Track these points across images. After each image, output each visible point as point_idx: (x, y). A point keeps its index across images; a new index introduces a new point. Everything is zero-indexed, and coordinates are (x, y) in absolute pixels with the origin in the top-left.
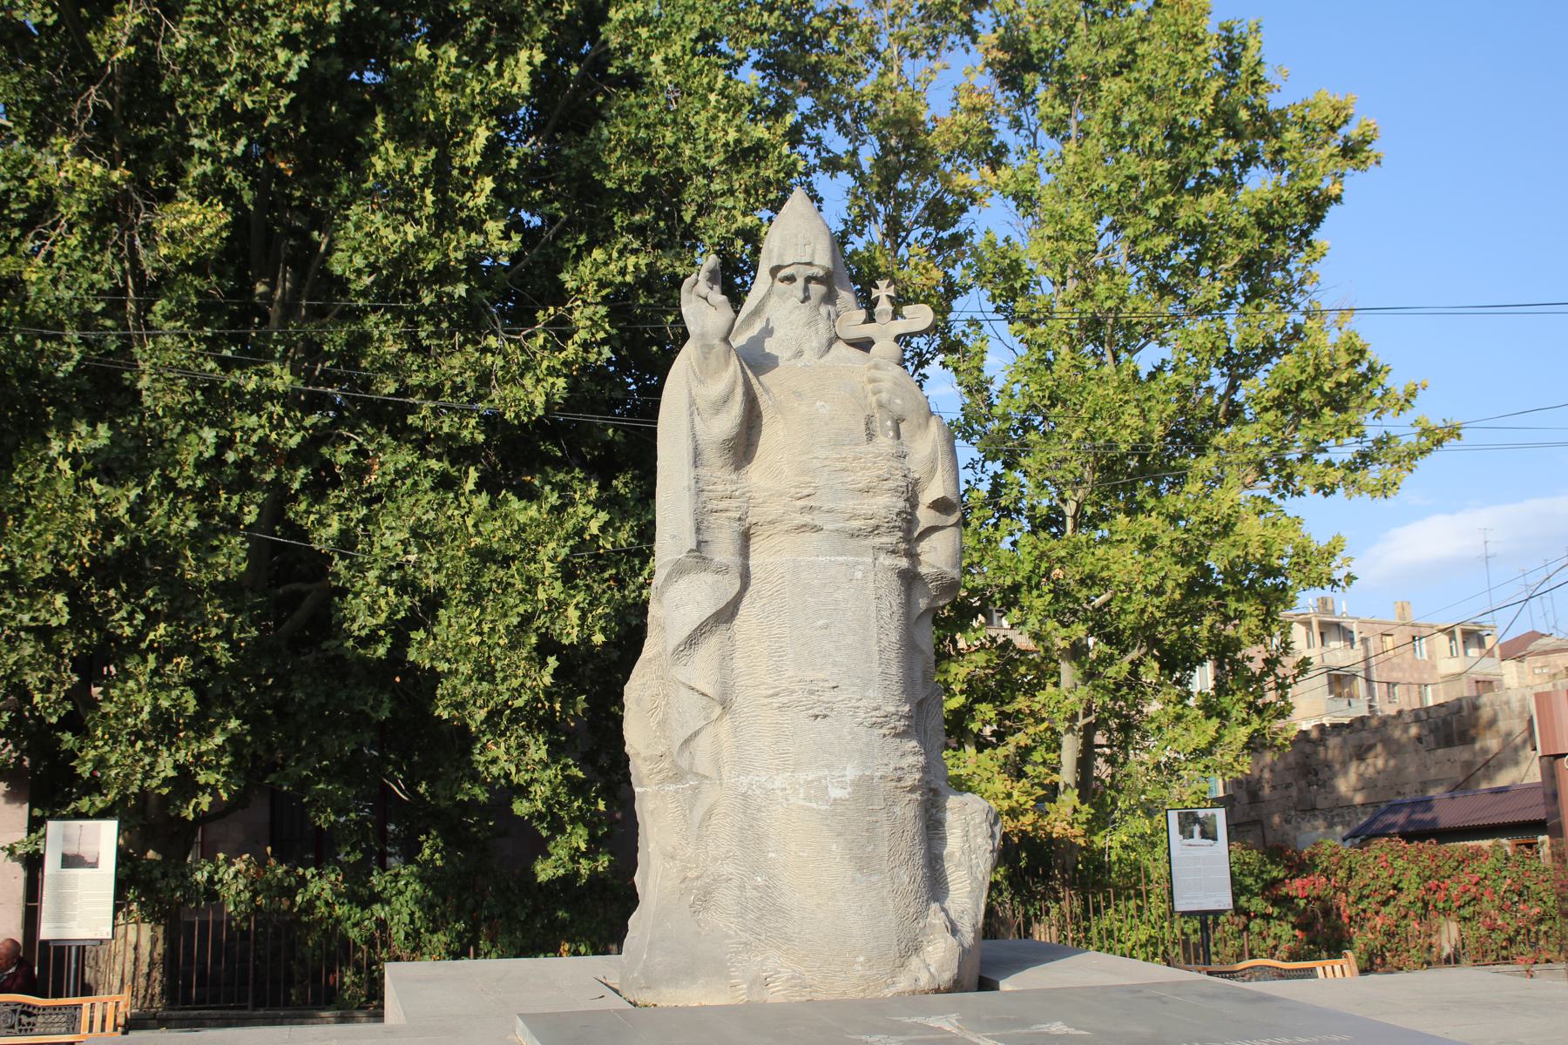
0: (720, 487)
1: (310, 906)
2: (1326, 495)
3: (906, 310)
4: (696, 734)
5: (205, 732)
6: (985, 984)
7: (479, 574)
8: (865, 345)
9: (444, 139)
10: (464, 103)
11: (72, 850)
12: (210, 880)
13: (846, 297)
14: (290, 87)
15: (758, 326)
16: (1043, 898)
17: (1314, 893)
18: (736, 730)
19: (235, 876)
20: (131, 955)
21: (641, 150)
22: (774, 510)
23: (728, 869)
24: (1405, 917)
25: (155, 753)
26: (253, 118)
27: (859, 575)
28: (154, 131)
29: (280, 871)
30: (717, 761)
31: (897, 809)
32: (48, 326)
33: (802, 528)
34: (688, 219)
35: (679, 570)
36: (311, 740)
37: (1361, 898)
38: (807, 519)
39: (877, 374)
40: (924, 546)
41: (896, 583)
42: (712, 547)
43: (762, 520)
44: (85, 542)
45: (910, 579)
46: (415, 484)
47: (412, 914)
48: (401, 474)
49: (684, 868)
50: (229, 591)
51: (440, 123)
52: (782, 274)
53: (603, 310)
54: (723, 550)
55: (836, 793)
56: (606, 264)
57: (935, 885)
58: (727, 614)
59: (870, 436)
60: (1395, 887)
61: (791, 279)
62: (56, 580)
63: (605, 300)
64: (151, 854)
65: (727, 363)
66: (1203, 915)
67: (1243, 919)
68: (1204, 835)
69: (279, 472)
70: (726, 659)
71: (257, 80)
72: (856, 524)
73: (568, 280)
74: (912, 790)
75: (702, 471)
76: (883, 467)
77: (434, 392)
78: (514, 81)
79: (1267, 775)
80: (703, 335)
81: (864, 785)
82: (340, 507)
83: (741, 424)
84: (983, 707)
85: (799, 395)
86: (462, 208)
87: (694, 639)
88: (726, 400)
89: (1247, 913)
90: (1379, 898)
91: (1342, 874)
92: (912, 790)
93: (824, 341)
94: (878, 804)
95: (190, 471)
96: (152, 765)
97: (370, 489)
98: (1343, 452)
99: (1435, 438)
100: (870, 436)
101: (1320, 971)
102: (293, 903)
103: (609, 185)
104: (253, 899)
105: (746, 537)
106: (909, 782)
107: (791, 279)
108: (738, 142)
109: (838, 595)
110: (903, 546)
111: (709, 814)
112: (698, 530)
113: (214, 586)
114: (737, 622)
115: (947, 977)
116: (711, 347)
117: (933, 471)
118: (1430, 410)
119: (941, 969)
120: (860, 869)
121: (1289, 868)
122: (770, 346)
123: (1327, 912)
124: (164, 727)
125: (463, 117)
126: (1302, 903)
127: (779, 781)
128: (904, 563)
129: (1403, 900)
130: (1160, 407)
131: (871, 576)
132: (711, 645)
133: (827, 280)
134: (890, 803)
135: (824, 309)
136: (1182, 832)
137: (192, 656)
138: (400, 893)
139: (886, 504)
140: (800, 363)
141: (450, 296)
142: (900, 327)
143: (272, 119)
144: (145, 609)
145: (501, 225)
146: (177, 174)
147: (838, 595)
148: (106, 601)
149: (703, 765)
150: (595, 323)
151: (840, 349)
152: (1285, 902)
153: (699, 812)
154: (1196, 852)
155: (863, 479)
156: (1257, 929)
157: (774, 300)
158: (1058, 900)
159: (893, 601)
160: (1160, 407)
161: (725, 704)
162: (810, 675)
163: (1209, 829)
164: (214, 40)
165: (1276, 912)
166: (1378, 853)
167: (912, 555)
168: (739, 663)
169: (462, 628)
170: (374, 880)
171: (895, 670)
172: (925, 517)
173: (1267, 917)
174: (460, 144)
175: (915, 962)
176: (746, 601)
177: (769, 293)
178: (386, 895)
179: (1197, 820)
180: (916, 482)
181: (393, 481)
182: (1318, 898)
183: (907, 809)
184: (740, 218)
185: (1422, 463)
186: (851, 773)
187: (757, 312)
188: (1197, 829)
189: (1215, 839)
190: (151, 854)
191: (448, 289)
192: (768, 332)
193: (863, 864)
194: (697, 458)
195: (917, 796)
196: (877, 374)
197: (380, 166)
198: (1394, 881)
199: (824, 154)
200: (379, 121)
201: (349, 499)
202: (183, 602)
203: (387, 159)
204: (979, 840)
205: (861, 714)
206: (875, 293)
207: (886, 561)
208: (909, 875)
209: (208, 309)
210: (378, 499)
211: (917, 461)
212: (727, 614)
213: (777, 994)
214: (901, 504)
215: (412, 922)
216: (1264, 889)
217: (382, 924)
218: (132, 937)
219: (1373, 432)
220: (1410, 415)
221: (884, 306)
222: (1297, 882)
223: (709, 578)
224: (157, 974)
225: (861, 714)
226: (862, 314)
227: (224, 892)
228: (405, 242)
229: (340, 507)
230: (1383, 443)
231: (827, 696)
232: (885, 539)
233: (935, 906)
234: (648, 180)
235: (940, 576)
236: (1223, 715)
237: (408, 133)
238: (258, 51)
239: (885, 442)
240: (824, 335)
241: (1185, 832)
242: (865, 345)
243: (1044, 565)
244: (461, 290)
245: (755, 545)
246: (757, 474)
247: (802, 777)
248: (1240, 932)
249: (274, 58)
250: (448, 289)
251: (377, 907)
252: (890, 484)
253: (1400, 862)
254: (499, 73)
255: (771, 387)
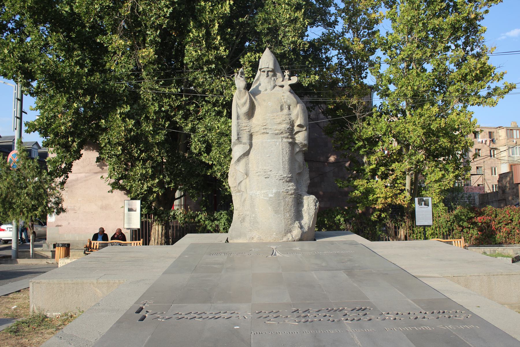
0: (244, 124)
1: (199, 221)
2: (478, 105)
3: (292, 78)
4: (241, 182)
5: (153, 179)
6: (315, 240)
7: (220, 139)
8: (282, 86)
9: (208, 27)
10: (213, 17)
11: (130, 207)
12: (174, 214)
13: (279, 75)
14: (168, 18)
15: (258, 83)
16: (401, 221)
17: (484, 221)
18: (250, 181)
19: (180, 214)
20: (157, 233)
21: (265, 20)
22: (257, 129)
23: (248, 213)
24: (514, 229)
25: (143, 184)
26: (160, 26)
27: (278, 144)
28: (140, 29)
29: (191, 213)
30: (246, 188)
31: (287, 199)
32: (119, 79)
33: (263, 133)
34: (280, 39)
35: (235, 144)
36: (188, 179)
37: (499, 223)
38: (265, 131)
39: (284, 94)
40: (296, 136)
41: (288, 145)
42: (242, 138)
43: (254, 131)
44: (123, 134)
45: (293, 144)
46: (210, 114)
47: (224, 223)
48: (207, 112)
49: (239, 213)
50: (160, 145)
51: (207, 23)
52: (262, 70)
53: (250, 69)
54: (245, 138)
55: (270, 195)
56: (251, 56)
57: (298, 216)
58: (247, 154)
59: (282, 109)
60: (511, 220)
61: (264, 71)
62: (119, 144)
63: (251, 66)
64: (161, 208)
65: (245, 94)
66: (424, 227)
67: (461, 228)
68: (425, 204)
69: (175, 113)
70: (247, 164)
71: (160, 17)
72: (277, 132)
73: (242, 61)
74: (291, 194)
75: (239, 121)
76: (284, 118)
77: (212, 91)
78: (225, 10)
79: (508, 185)
80: (239, 88)
81: (278, 194)
82: (192, 121)
83: (249, 109)
84: (381, 168)
85: (264, 100)
86: (213, 44)
87: (239, 160)
88: (245, 103)
89: (463, 227)
90: (505, 223)
91: (493, 216)
92: (291, 194)
93: (272, 87)
94: (281, 198)
95: (152, 114)
96: (143, 187)
97: (199, 116)
98: (483, 93)
99: (510, 88)
100: (282, 109)
101: (453, 242)
102: (195, 220)
103: (258, 31)
104: (185, 219)
105: (251, 136)
106: (290, 193)
107: (264, 71)
108: (290, 18)
109: (272, 149)
110: (290, 136)
111: (245, 200)
112: (238, 135)
113: (157, 144)
114: (250, 155)
115: (297, 238)
116: (241, 91)
117: (297, 118)
118: (507, 80)
119: (296, 236)
120: (276, 213)
121: (477, 214)
122: (260, 88)
123: (488, 226)
124: (144, 178)
125: (212, 21)
126: (480, 224)
127: (258, 193)
128: (290, 140)
129: (514, 224)
130: (424, 82)
131: (281, 144)
132: (243, 161)
133: (273, 71)
134: (284, 198)
135: (273, 78)
136: (419, 204)
137: (152, 160)
138: (221, 218)
139: (285, 126)
140: (266, 92)
141: (211, 68)
142: (290, 82)
143: (164, 26)
144: (140, 150)
145: (223, 48)
146: (144, 40)
147: (272, 149)
148: (131, 148)
149: (243, 189)
150: (249, 72)
151: (277, 88)
152: (475, 224)
153: (242, 200)
154: (422, 209)
155: (279, 121)
156: (466, 231)
157: (261, 76)
158: (405, 222)
159: (287, 149)
160: (424, 82)
161: (247, 174)
162: (265, 168)
163: (427, 203)
164: (149, 7)
165: (472, 226)
166: (506, 210)
167: (293, 138)
168: (250, 165)
169: (216, 153)
170: (215, 215)
171: (287, 166)
172: (296, 129)
173: (469, 228)
174: (212, 28)
175: (289, 234)
176: (252, 150)
177: (260, 75)
178: (218, 218)
179: (423, 200)
180: (293, 121)
181: (205, 114)
182: (485, 223)
183: (290, 200)
184: (291, 39)
185: (506, 96)
186: (274, 191)
187: (258, 79)
188: (423, 203)
189: (428, 206)
190: (161, 208)
191: (210, 66)
192: (260, 84)
193: (277, 212)
194: (238, 117)
195: (293, 196)
196: (284, 94)
197: (191, 35)
198: (511, 218)
199: (337, 9)
200: (191, 23)
201: (194, 119)
202: (148, 147)
203: (194, 33)
204: (312, 207)
205: (277, 177)
206: (285, 74)
207: (285, 140)
208: (289, 215)
209: (156, 73)
210: (202, 118)
211: (293, 117)
212: (247, 154)
213: (255, 240)
214: (289, 126)
215: (225, 225)
216: (467, 220)
217: (217, 226)
218: (157, 229)
219: (493, 86)
220: (501, 81)
221: (287, 77)
222: (478, 218)
223: (242, 146)
224: (163, 238)
225: (277, 177)
226: (281, 79)
227: (177, 217)
228: (199, 55)
229: (192, 121)
230: (495, 90)
231: (269, 173)
232: (285, 135)
233: (297, 222)
234: (268, 29)
235: (301, 143)
236: (447, 170)
237: (199, 26)
238: (160, 9)
239: (286, 111)
240: (272, 84)
241: (420, 204)
242: (282, 86)
243: (389, 129)
244: (213, 66)
245: (254, 137)
246: (254, 120)
247: (263, 192)
248: (461, 232)
249: (163, 11)
250: (210, 66)
251: (216, 222)
252: (286, 122)
253: (513, 213)
254: (222, 8)
255: (259, 100)
